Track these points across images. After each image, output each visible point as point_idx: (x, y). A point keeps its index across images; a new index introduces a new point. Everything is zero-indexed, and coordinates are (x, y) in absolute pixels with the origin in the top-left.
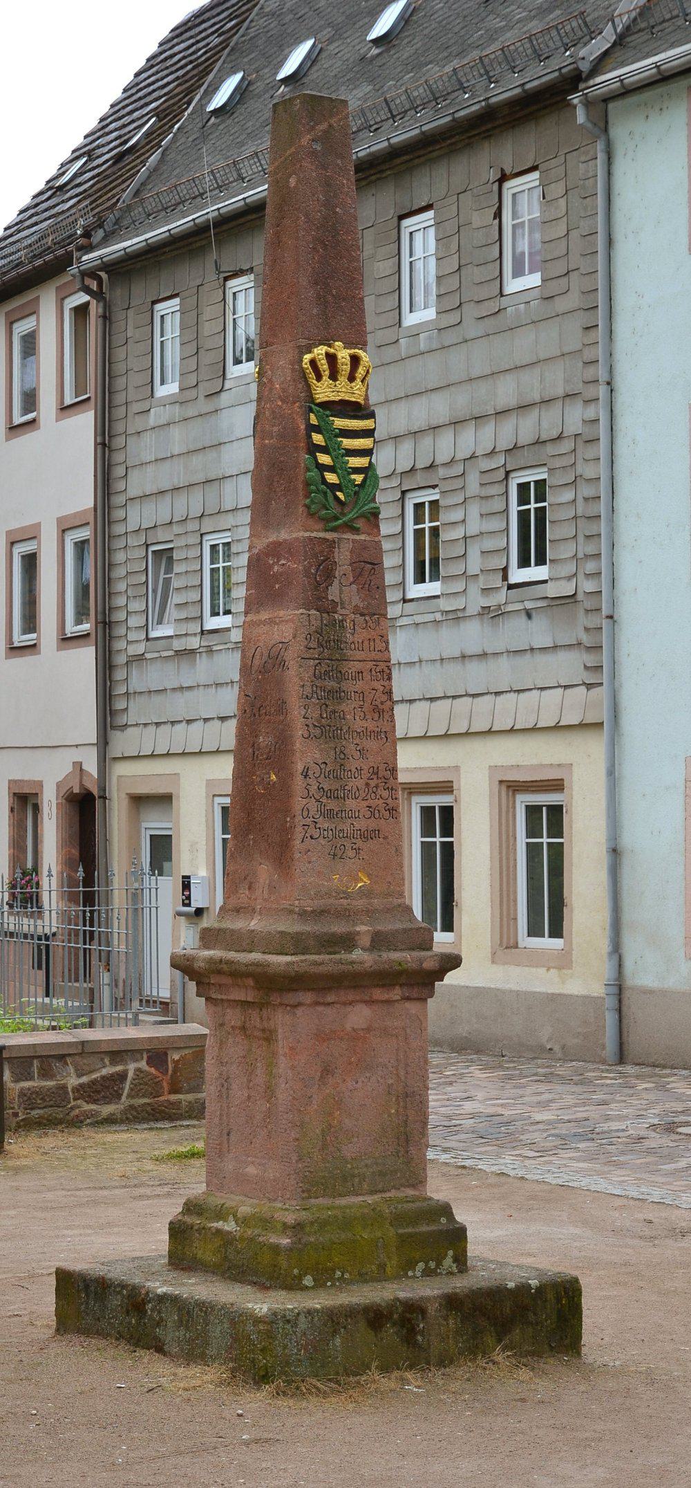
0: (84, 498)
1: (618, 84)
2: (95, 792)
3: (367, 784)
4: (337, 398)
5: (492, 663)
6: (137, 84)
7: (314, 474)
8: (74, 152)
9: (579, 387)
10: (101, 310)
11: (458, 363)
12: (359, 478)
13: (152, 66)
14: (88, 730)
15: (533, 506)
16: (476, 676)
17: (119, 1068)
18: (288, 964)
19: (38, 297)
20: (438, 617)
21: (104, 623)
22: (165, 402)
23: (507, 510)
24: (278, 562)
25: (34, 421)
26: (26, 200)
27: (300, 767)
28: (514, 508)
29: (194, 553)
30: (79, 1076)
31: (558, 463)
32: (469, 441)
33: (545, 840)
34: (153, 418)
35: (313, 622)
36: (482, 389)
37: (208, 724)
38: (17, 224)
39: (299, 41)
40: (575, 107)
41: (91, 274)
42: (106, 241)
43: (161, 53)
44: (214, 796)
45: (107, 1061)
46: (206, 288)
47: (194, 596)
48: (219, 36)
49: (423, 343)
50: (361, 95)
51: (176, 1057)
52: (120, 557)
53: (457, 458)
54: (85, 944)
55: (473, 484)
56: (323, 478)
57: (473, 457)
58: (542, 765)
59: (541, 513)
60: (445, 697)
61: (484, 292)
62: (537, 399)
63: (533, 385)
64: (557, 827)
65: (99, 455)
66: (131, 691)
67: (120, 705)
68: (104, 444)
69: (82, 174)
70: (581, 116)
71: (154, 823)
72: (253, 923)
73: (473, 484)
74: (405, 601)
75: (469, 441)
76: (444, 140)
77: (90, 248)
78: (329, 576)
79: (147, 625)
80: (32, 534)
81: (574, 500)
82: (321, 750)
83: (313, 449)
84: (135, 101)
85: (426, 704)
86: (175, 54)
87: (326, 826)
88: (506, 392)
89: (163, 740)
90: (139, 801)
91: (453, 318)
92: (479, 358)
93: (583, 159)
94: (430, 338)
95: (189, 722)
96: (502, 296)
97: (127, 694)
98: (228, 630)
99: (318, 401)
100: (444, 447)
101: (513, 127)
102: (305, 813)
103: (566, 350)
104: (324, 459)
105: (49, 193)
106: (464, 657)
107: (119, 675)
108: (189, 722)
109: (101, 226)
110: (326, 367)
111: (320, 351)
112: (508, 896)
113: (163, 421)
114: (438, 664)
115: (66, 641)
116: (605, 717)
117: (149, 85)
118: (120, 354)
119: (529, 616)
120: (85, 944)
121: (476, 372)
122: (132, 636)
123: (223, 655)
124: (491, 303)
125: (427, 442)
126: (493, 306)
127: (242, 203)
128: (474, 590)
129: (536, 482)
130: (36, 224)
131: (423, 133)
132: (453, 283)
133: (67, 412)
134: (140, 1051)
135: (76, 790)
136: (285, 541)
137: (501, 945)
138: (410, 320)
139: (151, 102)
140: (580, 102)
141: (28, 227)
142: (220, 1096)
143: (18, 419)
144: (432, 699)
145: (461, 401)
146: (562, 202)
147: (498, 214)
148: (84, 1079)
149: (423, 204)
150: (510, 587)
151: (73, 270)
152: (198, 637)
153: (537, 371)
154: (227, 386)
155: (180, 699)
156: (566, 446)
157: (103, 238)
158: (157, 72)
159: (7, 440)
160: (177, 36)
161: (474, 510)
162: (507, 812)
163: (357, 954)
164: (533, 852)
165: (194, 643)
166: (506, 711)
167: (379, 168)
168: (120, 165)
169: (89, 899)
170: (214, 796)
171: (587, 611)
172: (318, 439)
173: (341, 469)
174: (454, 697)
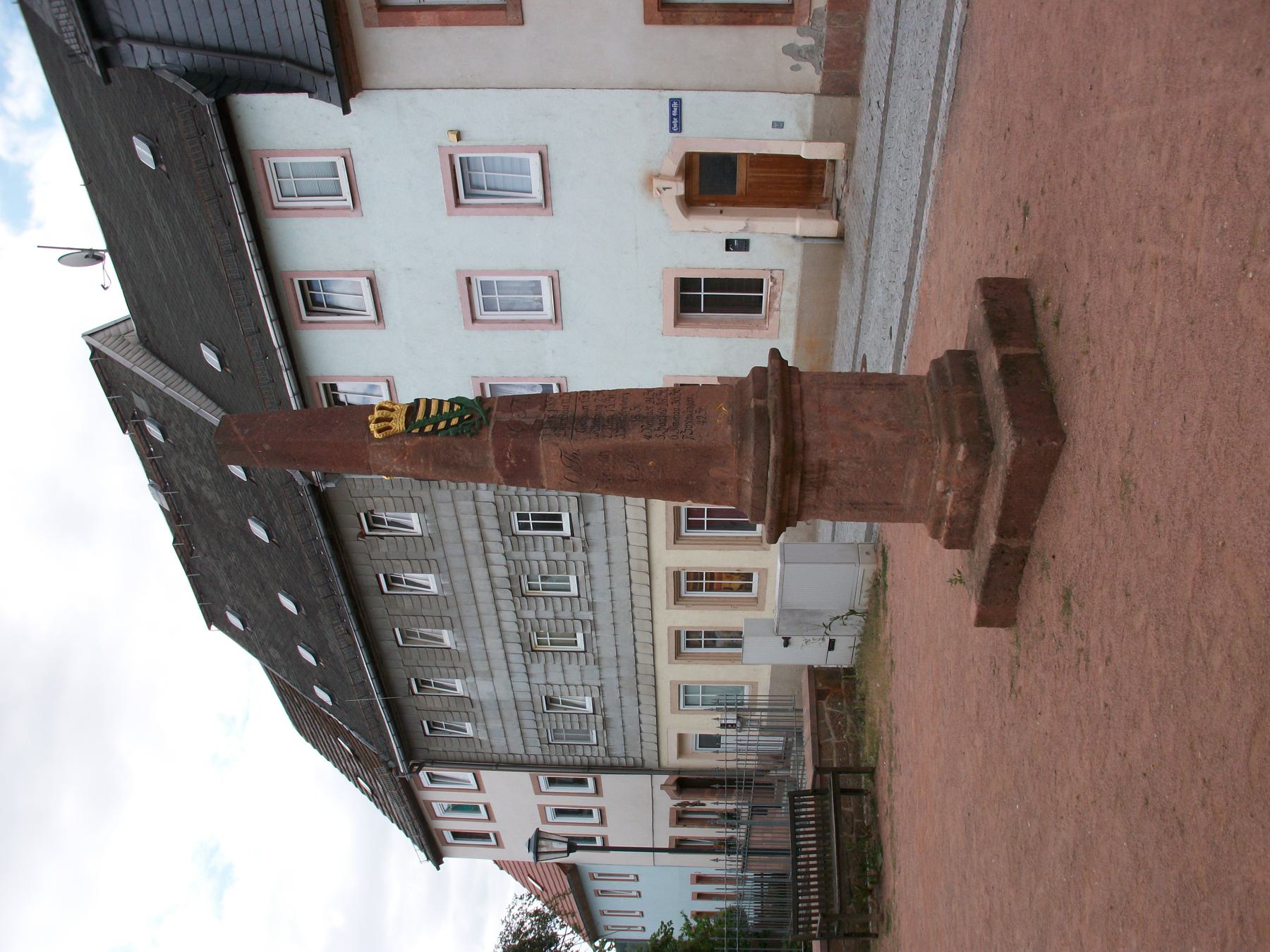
0: (524, 777)
2: (676, 777)
3: (657, 404)
4: (404, 418)
5: (612, 547)
6: (325, 753)
7: (450, 431)
8: (356, 787)
10: (429, 765)
11: (457, 563)
12: (456, 407)
13: (317, 745)
14: (644, 779)
15: (531, 521)
16: (619, 555)
17: (827, 715)
18: (776, 440)
19: (424, 801)
20: (588, 577)
21: (589, 769)
22: (476, 732)
23: (532, 536)
24: (507, 459)
25: (495, 835)
26: (379, 812)
27: (644, 440)
28: (532, 532)
29: (553, 717)
30: (831, 736)
31: (508, 505)
32: (497, 558)
33: (706, 519)
34: (484, 737)
35: (548, 432)
36: (469, 548)
37: (641, 711)
38: (390, 816)
39: (299, 655)
41: (410, 770)
42: (395, 760)
43: (311, 741)
44: (679, 709)
45: (822, 721)
46: (417, 705)
47: (575, 718)
48: (301, 706)
50: (323, 616)
51: (820, 685)
52: (555, 759)
53: (505, 564)
54: (752, 784)
55: (519, 555)
56: (453, 426)
57: (505, 555)
58: (666, 518)
59: (535, 517)
60: (630, 574)
61: (421, 547)
62: (475, 517)
63: (468, 519)
64: (698, 576)
65: (501, 768)
66: (624, 755)
67: (631, 761)
68: (497, 766)
69: (366, 780)
70: (331, 485)
71: (692, 744)
72: (748, 480)
73: (519, 555)
74: (579, 596)
75: (497, 558)
76: (343, 565)
77: (397, 768)
78: (518, 424)
79: (590, 745)
80: (542, 809)
81: (528, 496)
82: (633, 428)
83: (435, 431)
84: (332, 752)
85: (633, 585)
86: (311, 732)
88: (472, 535)
89: (649, 738)
90: (681, 752)
91: (433, 564)
92: (454, 550)
93: (354, 487)
94: (443, 578)
95: (640, 722)
97: (626, 757)
98: (593, 699)
99: (404, 428)
100: (500, 571)
101: (342, 541)
102: (675, 438)
103: (450, 499)
104: (442, 425)
105: (375, 798)
106: (609, 563)
107: (616, 761)
108: (640, 722)
109: (387, 762)
110: (383, 423)
111: (372, 427)
112: (733, 541)
113: (485, 732)
114: (611, 565)
115: (598, 792)
117: (325, 745)
118: (451, 755)
120: (752, 784)
121: (461, 552)
122: (596, 754)
123: (606, 702)
124: (426, 542)
125: (496, 581)
126: (428, 542)
127: (363, 649)
128: (574, 556)
129: (518, 520)
130: (389, 804)
131: (339, 575)
132: (415, 563)
133: (481, 787)
134: (817, 704)
135: (675, 788)
136: (494, 453)
137: (759, 545)
138: (434, 589)
139: (332, 743)
140: (324, 484)
141: (391, 808)
142: (863, 510)
143: (494, 842)
144: (631, 582)
145: (476, 562)
146: (375, 499)
147: (381, 537)
148: (832, 734)
149: (376, 579)
150: (573, 535)
151: (408, 777)
152: (597, 716)
153: (461, 517)
154: (468, 696)
155: (628, 727)
156: (500, 500)
157: (393, 761)
158: (319, 741)
159: (495, 822)
160: (303, 732)
161: (533, 555)
162: (690, 540)
163: (770, 406)
164: (712, 526)
165: (599, 718)
166: (637, 540)
167: (358, 603)
168: (360, 758)
169: (731, 781)
170: (679, 709)
172: (428, 429)
173: (449, 416)
174: (630, 569)
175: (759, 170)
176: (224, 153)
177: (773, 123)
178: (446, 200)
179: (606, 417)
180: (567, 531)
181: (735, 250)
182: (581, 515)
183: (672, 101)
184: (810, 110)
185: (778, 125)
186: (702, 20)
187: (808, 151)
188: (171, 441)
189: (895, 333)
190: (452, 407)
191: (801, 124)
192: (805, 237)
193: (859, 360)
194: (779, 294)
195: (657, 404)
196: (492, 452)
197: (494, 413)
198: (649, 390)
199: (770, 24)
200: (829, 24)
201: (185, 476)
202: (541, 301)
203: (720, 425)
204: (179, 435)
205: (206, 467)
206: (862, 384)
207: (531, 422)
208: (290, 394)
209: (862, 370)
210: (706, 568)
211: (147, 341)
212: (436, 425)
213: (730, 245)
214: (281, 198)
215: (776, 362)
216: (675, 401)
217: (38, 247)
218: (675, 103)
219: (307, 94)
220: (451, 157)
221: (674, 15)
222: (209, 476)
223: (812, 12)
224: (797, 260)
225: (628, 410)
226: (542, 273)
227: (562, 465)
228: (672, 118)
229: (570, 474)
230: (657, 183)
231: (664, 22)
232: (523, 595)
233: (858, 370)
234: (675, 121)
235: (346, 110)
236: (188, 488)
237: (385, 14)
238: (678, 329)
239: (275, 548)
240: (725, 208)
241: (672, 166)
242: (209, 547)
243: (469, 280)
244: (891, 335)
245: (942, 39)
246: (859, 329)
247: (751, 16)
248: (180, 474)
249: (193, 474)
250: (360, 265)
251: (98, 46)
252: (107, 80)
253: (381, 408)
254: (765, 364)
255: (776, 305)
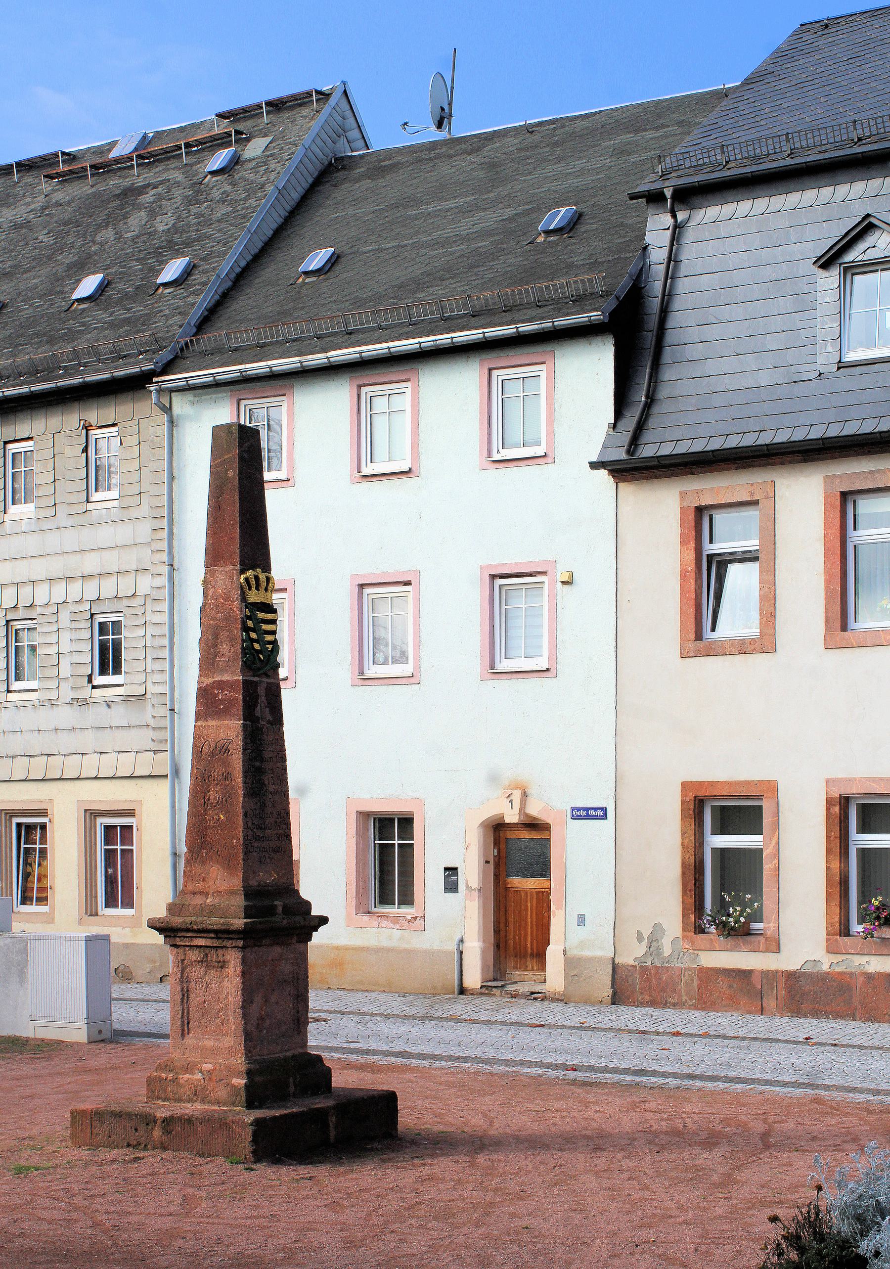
1: (185, 383)
3: (276, 822)
9: (148, 565)
12: (270, 647)
20: (37, 703)
36: (74, 559)
40: (151, 392)
49: (24, 526)
55: (65, 617)
56: (253, 645)
63: (112, 560)
72: (208, 901)
87: (256, 845)
88: (91, 564)
92: (70, 539)
94: (30, 523)
96: (88, 502)
104: (253, 635)
111: (250, 573)
116: (167, 770)
119: (109, 706)
124: (80, 506)
128: (65, 687)
129: (113, 622)
137: (86, 913)
145: (57, 567)
147: (85, 450)
156: (139, 601)
162: (91, 829)
163: (277, 918)
164: (110, 855)
171: (154, 706)
175: (535, 901)
176: (550, 324)
177: (584, 915)
178: (498, 565)
179: (263, 778)
180: (99, 680)
181: (446, 878)
182: (121, 698)
183: (604, 810)
184: (599, 953)
185: (581, 920)
186: (686, 840)
187: (554, 953)
188: (207, 180)
189: (352, 1046)
190: (270, 643)
191: (582, 945)
192: (462, 952)
193: (323, 1015)
194: (398, 926)
195: (276, 822)
196: (229, 678)
197: (265, 680)
198: (288, 813)
199: (684, 909)
200: (686, 969)
201: (160, 190)
202: (386, 662)
203: (259, 876)
204: (216, 194)
205: (174, 225)
206: (298, 996)
207: (258, 713)
208: (270, 363)
209: (311, 1018)
210: (53, 849)
211: (337, 168)
212: (254, 630)
213: (451, 871)
214: (501, 378)
215: (316, 922)
216: (279, 836)
217: (455, 50)
218: (601, 813)
219: (612, 421)
220: (545, 573)
221: (691, 812)
222: (162, 225)
223: (696, 952)
224: (436, 946)
225: (270, 796)
226: (418, 666)
227: (218, 739)
228: (586, 809)
229: (210, 746)
230: (517, 795)
231: (683, 802)
232: (8, 621)
233: (311, 1015)
234: (584, 813)
235: (594, 466)
236: (142, 190)
237: (692, 515)
238: (354, 816)
239: (65, 305)
240: (491, 866)
241: (534, 810)
242: (58, 204)
243: (407, 583)
244: (350, 1042)
245: (641, 1070)
246: (359, 1013)
247: (690, 890)
248: (161, 183)
249: (163, 203)
250: (426, 462)
251: (668, 193)
252: (633, 197)
253: (268, 579)
254: (315, 912)
255: (384, 923)
